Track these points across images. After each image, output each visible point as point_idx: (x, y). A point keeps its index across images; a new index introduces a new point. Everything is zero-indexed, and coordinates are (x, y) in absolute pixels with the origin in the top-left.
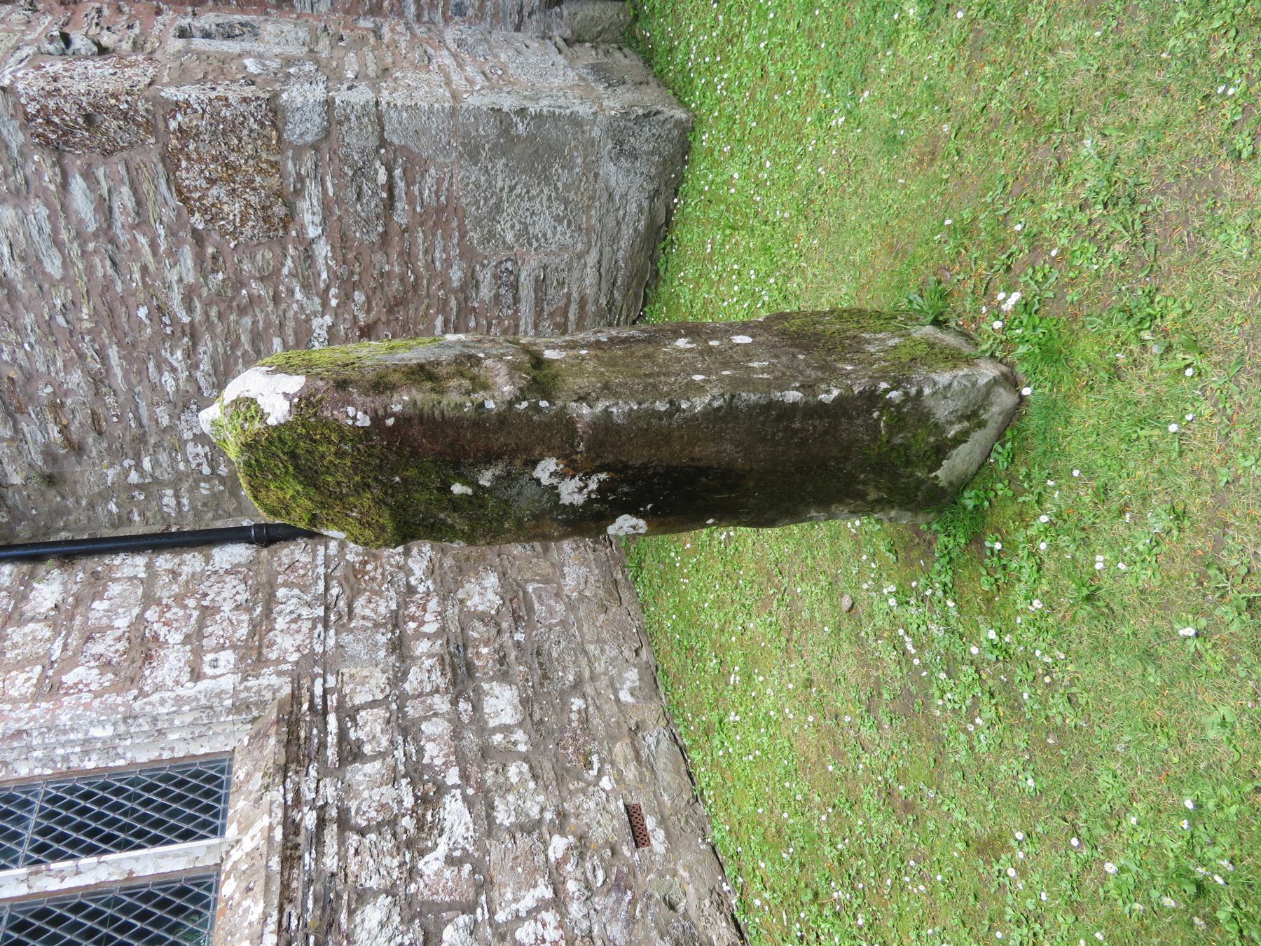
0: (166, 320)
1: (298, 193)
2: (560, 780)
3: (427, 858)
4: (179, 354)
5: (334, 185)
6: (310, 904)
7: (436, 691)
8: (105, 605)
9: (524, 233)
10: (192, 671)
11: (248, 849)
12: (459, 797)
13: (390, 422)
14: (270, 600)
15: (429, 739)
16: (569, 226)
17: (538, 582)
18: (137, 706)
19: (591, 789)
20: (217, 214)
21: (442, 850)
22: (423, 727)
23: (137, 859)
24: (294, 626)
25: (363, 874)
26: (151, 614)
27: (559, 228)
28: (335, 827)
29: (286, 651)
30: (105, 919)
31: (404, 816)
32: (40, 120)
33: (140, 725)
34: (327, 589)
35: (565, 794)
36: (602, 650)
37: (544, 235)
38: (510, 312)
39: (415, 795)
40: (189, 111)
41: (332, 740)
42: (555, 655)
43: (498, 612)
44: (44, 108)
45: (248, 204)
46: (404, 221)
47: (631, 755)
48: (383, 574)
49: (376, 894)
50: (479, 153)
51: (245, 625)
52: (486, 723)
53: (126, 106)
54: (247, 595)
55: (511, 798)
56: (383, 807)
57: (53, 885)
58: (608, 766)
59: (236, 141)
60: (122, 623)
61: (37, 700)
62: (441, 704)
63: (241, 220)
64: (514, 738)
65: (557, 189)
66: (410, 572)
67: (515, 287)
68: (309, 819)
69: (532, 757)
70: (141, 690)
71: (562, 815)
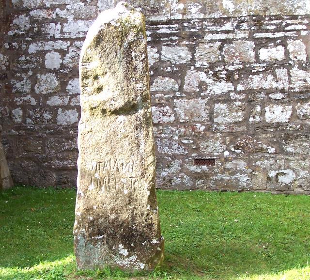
21: (208, 81)
22: (270, 75)
41: (270, 35)
42: (305, 144)
58: (234, 156)
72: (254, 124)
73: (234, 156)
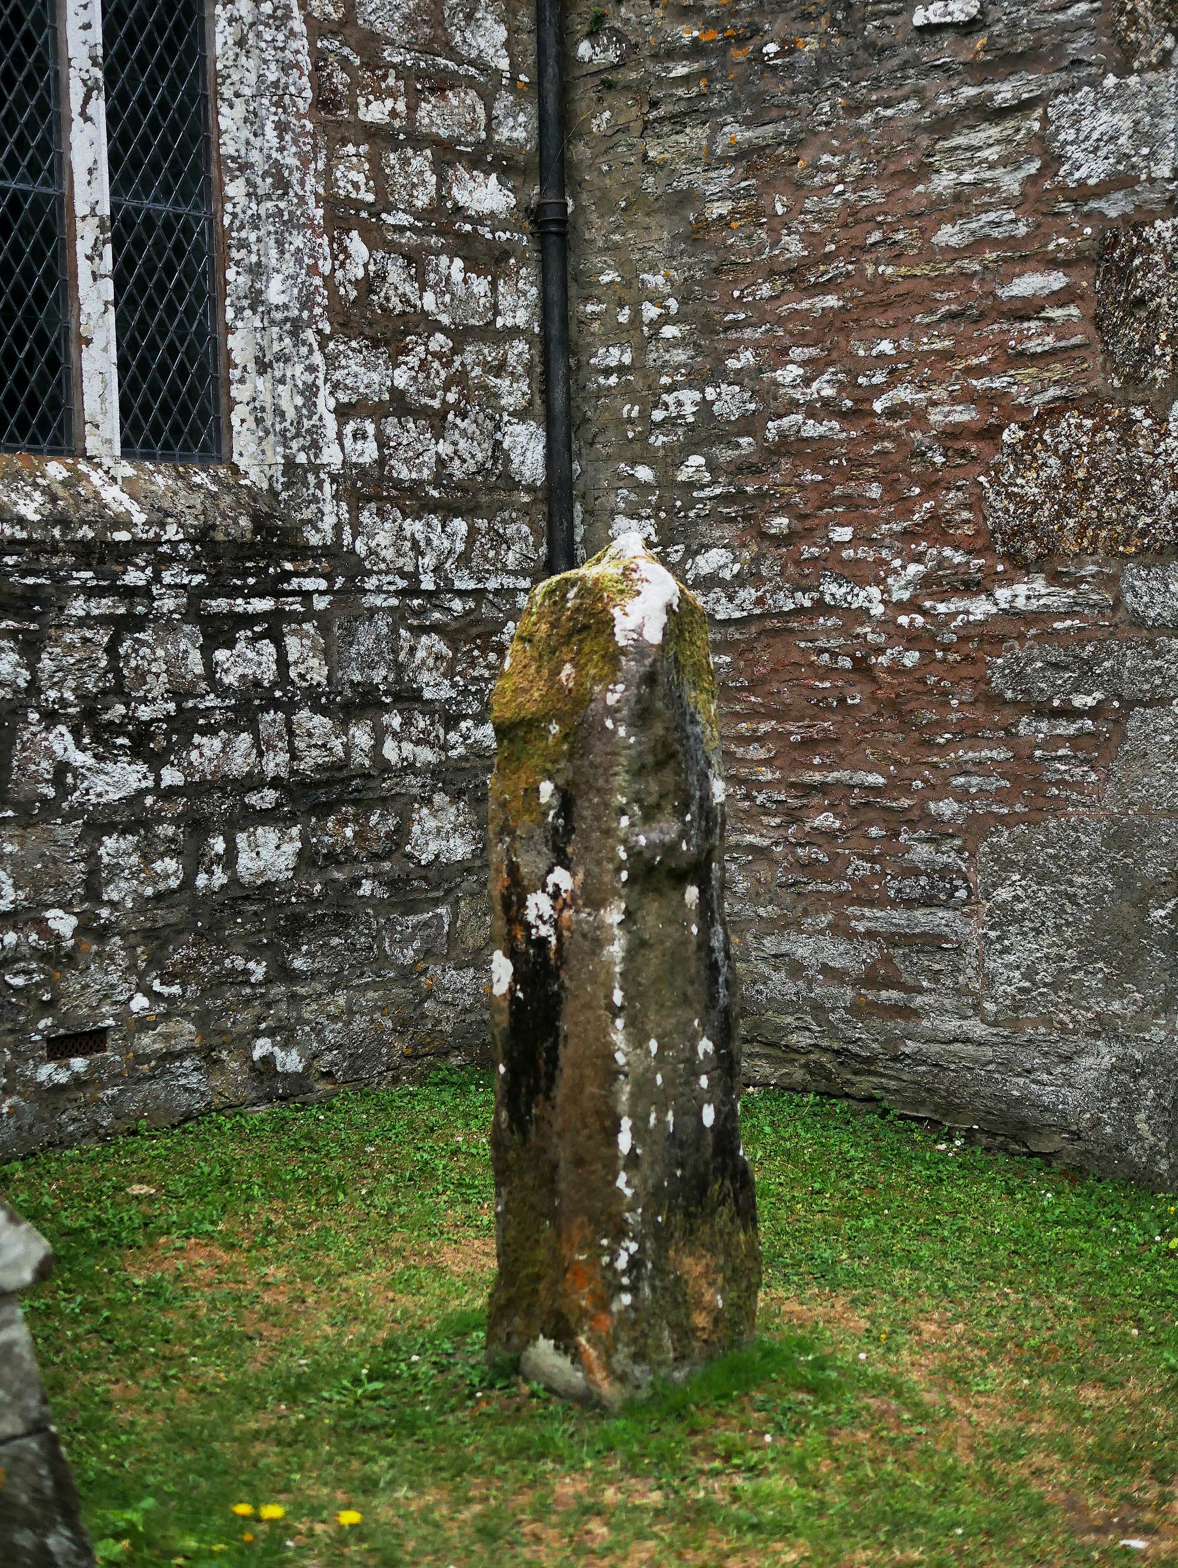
0: (879, 379)
1: (1055, 578)
2: (149, 934)
3: (69, 737)
4: (828, 392)
5: (1067, 629)
6: (30, 581)
7: (294, 755)
8: (457, 276)
9: (1005, 917)
10: (349, 405)
11: (103, 495)
12: (144, 784)
13: (609, 724)
14: (448, 511)
15: (226, 744)
16: (1022, 990)
17: (452, 924)
18: (309, 335)
19: (134, 979)
20: (1023, 462)
21: (80, 759)
22: (244, 735)
23: (105, 350)
24: (408, 545)
25: (59, 650)
26: (439, 341)
27: (1017, 974)
28: (122, 610)
29: (372, 536)
30: (33, 313)
31: (127, 705)
32: (1135, 241)
33: (281, 339)
34: (462, 594)
35: (133, 939)
36: (333, 1018)
37: (1006, 950)
38: (892, 893)
39: (153, 721)
40: (1156, 436)
41: (240, 605)
42: (335, 941)
43: (410, 857)
44: (1151, 249)
45: (1036, 506)
46: (1022, 730)
47: (179, 1045)
48: (481, 678)
49: (31, 667)
50: (1120, 848)
51: (414, 476)
52: (243, 830)
53: (1158, 353)
54: (458, 475)
55: (135, 859)
56: (141, 676)
57: (83, 247)
58: (162, 1008)
59: (1119, 496)
60: (429, 301)
61: (326, 200)
62: (275, 763)
63: (1016, 494)
64: (218, 870)
65: (1074, 970)
66: (480, 720)
67: (928, 901)
68: (134, 577)
69: (186, 895)
70: (330, 337)
71: (103, 933)
72: (209, 891)
73: (162, 1008)
